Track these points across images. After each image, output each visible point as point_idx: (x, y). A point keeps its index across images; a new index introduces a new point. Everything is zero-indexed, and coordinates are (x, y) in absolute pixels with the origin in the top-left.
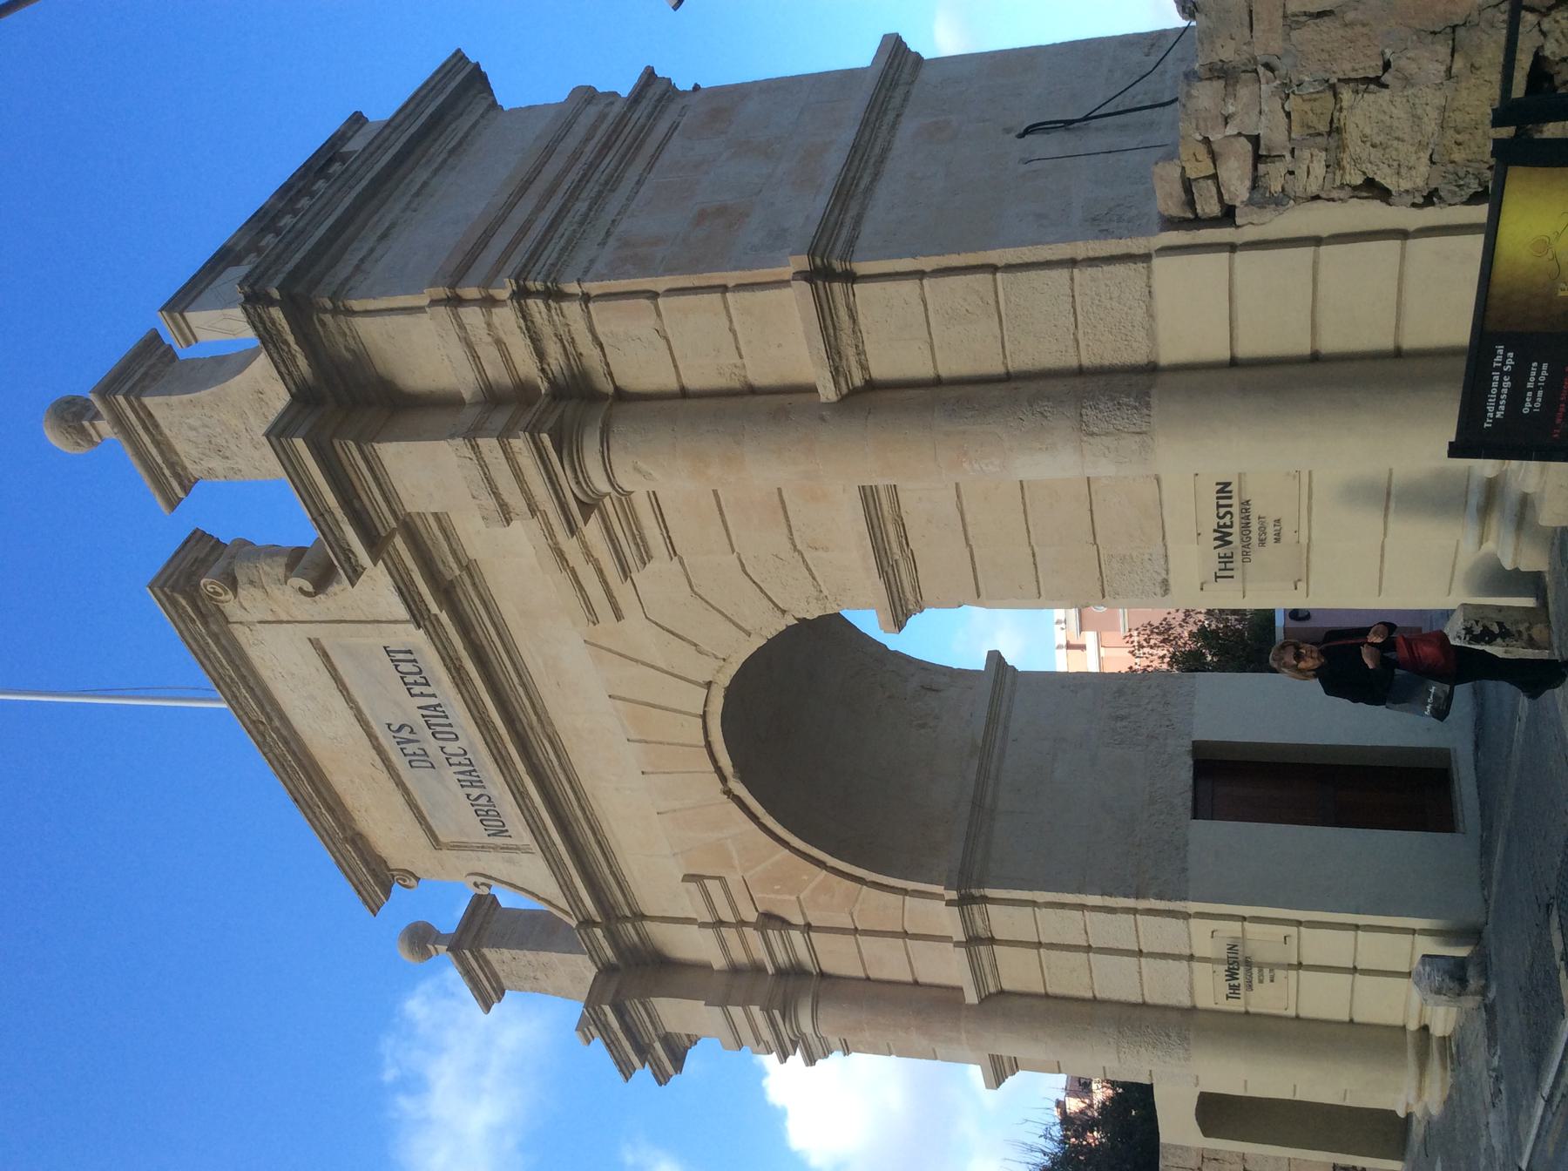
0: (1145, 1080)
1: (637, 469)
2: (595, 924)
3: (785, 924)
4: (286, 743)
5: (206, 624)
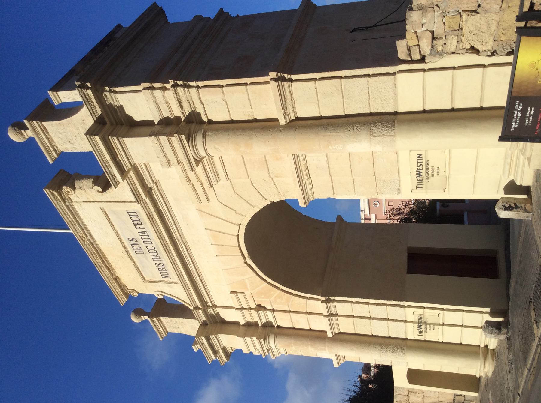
2: (199, 308)
4: (92, 244)
5: (65, 202)
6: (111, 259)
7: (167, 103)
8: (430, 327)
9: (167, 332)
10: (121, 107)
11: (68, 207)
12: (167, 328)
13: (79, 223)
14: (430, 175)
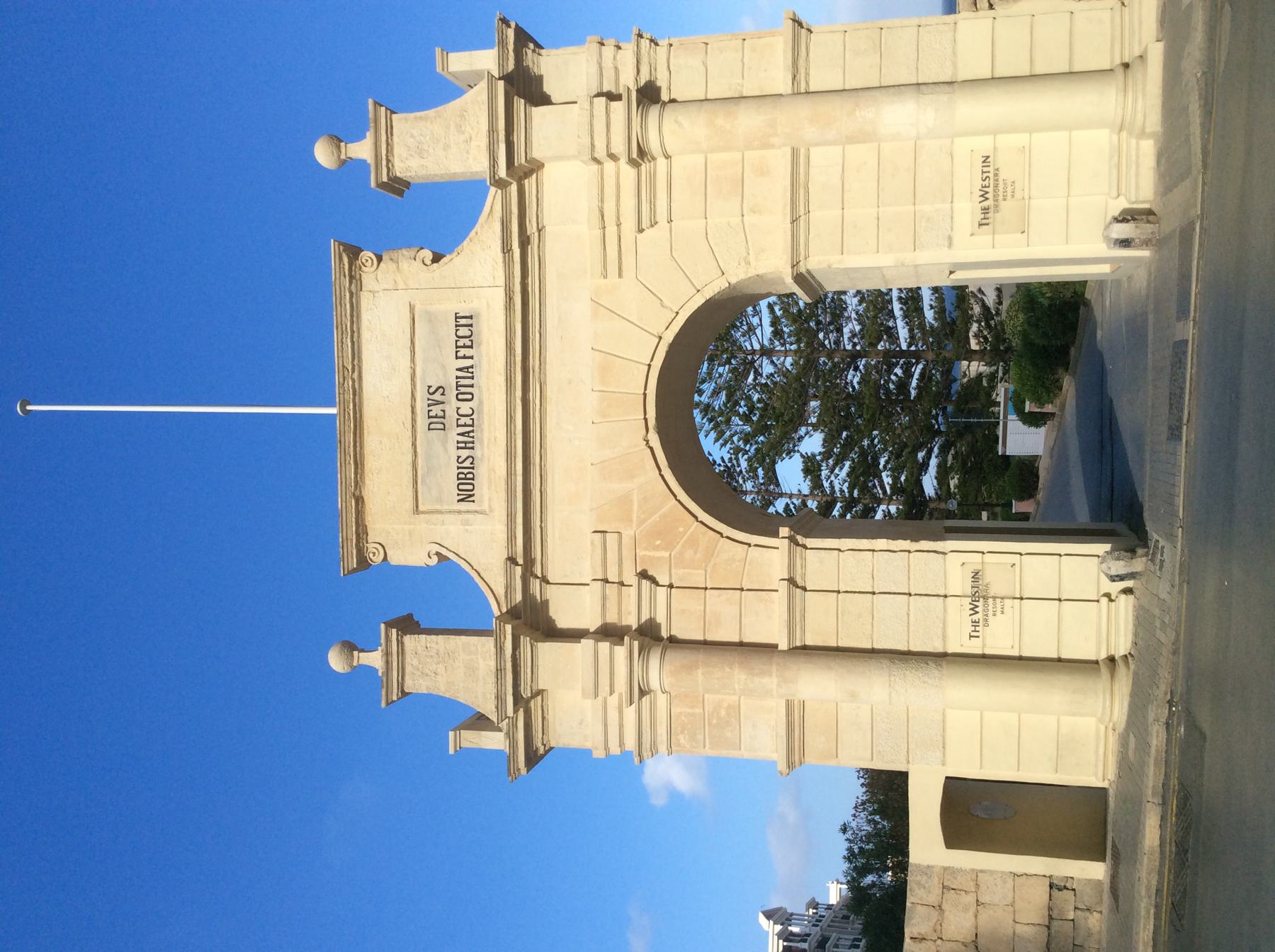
0: (904, 770)
2: (517, 564)
3: (654, 581)
4: (354, 395)
5: (351, 283)
6: (372, 442)
7: (616, 68)
8: (995, 604)
9: (403, 691)
10: (541, 77)
11: (351, 294)
12: (407, 678)
14: (1001, 198)
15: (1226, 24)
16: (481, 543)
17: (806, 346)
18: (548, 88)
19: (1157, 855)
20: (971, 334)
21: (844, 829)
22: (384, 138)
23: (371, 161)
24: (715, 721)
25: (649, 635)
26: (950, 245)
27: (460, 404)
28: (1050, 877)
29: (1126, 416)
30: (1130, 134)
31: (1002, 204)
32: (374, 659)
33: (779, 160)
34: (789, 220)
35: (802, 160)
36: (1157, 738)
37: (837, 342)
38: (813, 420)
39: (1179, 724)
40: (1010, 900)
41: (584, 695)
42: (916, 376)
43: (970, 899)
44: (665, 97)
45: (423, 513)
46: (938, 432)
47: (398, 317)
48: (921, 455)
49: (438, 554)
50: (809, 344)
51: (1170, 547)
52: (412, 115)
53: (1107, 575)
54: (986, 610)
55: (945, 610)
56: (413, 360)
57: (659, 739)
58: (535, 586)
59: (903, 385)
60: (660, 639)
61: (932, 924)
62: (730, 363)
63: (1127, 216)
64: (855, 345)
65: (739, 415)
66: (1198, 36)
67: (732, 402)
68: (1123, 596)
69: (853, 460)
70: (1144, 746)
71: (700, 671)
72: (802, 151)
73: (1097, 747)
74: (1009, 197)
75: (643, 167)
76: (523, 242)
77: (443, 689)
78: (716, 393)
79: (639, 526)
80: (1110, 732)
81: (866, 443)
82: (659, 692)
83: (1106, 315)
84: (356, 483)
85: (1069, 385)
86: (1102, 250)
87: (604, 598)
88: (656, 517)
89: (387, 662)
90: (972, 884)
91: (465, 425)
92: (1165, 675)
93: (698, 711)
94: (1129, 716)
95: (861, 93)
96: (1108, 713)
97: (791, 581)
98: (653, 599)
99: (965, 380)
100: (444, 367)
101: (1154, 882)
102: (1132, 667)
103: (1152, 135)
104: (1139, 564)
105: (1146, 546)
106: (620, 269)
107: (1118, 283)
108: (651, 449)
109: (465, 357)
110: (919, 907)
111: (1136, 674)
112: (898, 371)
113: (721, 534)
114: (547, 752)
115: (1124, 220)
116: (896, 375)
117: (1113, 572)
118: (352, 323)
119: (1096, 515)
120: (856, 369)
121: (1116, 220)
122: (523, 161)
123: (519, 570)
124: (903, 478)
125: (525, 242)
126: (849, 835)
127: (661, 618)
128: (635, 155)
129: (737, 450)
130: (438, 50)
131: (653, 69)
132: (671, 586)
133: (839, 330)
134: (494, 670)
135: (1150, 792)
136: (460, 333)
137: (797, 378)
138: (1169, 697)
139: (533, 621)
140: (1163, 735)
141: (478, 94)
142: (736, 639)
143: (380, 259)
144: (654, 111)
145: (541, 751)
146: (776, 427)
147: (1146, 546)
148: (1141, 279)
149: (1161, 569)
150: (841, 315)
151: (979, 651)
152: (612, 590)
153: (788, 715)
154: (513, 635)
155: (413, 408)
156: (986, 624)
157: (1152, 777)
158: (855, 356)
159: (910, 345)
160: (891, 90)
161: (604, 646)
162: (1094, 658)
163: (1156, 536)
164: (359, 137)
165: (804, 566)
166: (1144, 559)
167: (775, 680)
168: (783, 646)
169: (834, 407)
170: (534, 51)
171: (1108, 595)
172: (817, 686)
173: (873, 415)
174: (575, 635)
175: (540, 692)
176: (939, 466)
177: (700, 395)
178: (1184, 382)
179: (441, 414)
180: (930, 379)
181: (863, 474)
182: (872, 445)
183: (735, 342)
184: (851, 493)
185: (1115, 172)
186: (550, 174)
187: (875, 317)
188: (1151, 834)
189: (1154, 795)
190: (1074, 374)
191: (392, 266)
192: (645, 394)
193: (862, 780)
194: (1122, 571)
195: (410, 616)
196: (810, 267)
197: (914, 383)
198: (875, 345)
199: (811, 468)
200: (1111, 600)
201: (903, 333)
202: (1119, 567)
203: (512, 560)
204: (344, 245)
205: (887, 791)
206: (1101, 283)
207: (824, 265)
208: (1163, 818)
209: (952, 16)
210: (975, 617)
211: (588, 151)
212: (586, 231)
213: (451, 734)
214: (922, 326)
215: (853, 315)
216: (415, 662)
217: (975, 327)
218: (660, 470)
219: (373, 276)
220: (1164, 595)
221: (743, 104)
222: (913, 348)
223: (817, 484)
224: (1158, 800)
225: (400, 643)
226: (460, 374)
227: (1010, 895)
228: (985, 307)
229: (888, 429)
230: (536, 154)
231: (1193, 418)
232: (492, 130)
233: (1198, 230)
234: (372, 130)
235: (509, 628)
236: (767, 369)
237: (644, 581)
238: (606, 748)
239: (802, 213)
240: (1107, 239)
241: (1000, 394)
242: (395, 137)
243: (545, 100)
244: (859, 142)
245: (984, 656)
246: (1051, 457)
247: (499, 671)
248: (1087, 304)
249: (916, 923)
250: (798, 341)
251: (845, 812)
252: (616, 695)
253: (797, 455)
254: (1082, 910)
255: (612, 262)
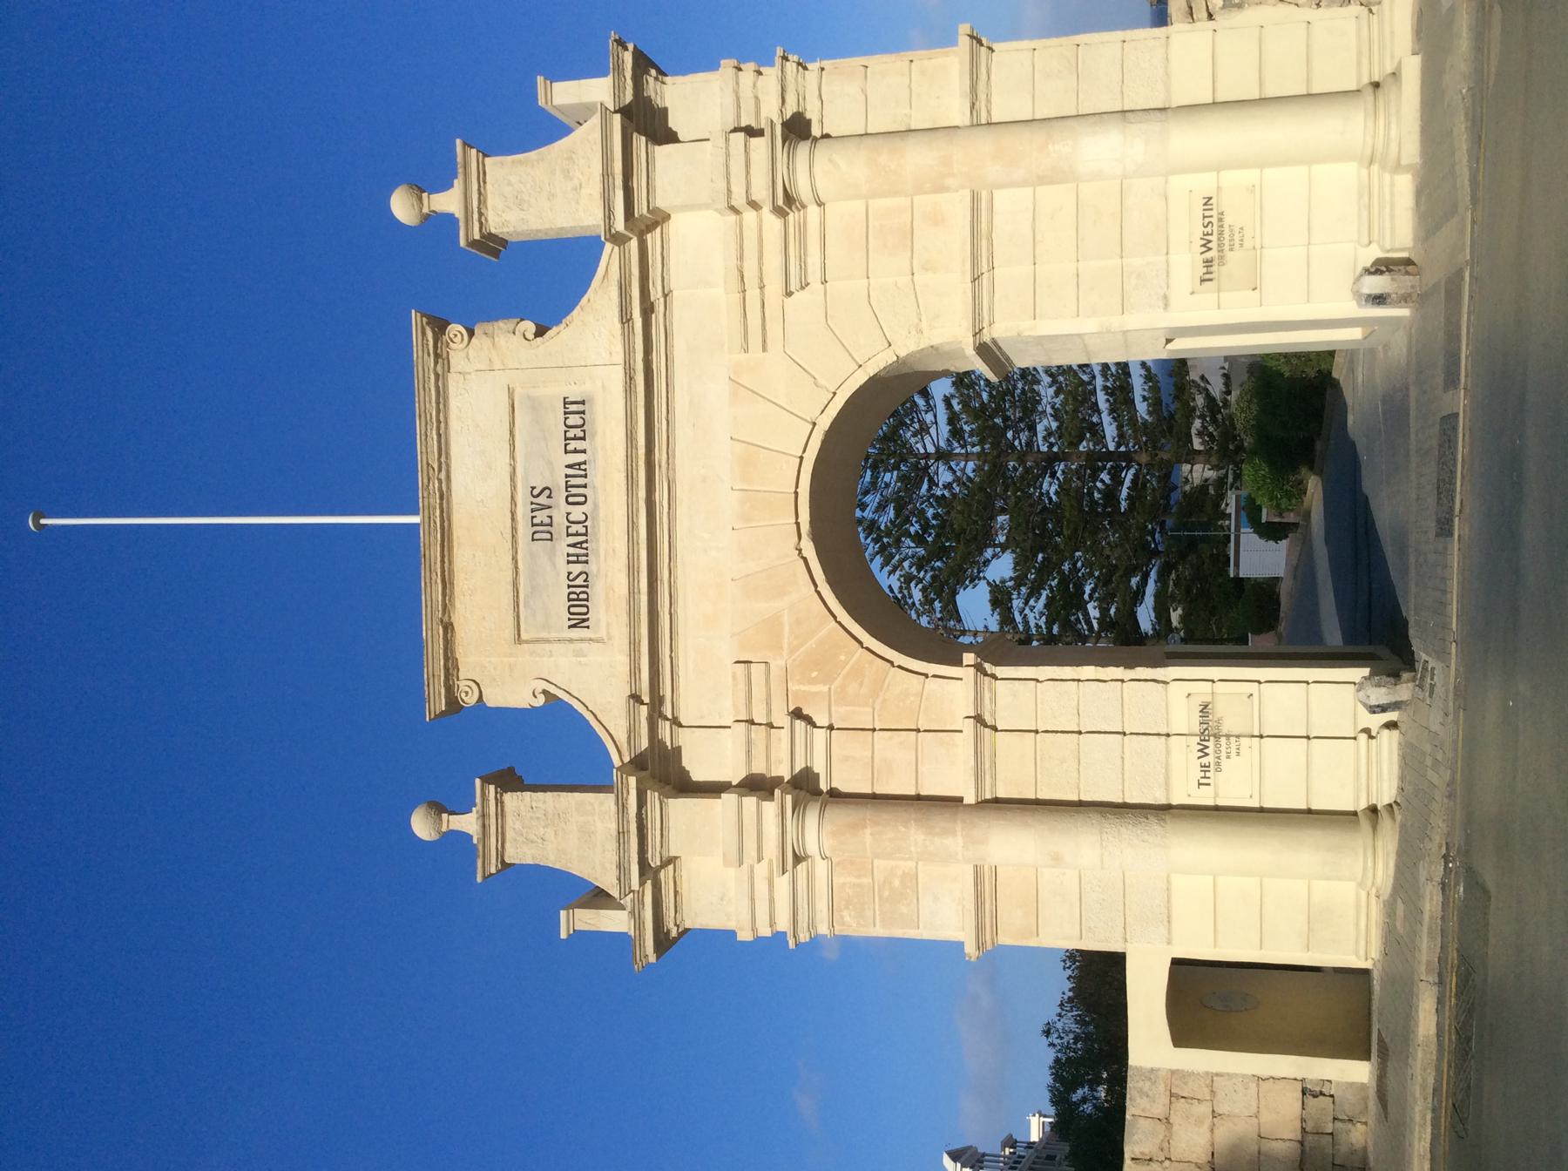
1: (830, 161)
3: (809, 720)
4: (441, 498)
5: (436, 363)
8: (1228, 744)
9: (503, 862)
10: (666, 109)
12: (508, 845)
13: (438, 428)
14: (1227, 247)
15: (1496, 31)
16: (597, 680)
17: (992, 448)
18: (673, 123)
19: (1434, 1047)
20: (1193, 432)
21: (1047, 1033)
22: (475, 187)
23: (459, 214)
24: (887, 893)
25: (805, 787)
26: (1166, 306)
27: (570, 508)
28: (1303, 1080)
29: (1385, 514)
30: (1383, 167)
31: (1229, 255)
32: (467, 823)
33: (956, 206)
34: (968, 278)
35: (984, 205)
36: (1431, 902)
37: (1030, 444)
38: (1002, 539)
39: (1457, 884)
40: (1254, 1109)
41: (726, 863)
42: (1127, 483)
43: (1205, 1109)
44: (816, 131)
45: (527, 642)
46: (1156, 553)
47: (490, 400)
48: (1134, 581)
49: (545, 692)
50: (995, 445)
51: (1442, 666)
52: (510, 158)
53: (1365, 705)
54: (1217, 751)
55: (1168, 752)
56: (512, 457)
57: (818, 916)
58: (665, 730)
59: (1111, 494)
60: (818, 793)
61: (1158, 1141)
62: (898, 468)
63: (1382, 267)
64: (1051, 445)
65: (908, 535)
66: (1463, 44)
67: (902, 518)
68: (1386, 732)
69: (1051, 588)
70: (1415, 913)
71: (868, 831)
72: (984, 195)
73: (1357, 942)
74: (1237, 246)
75: (791, 216)
76: (645, 309)
77: (552, 858)
78: (881, 507)
79: (792, 652)
80: (1373, 900)
81: (1066, 567)
82: (818, 858)
83: (1359, 393)
84: (445, 606)
85: (1314, 486)
86: (1352, 309)
87: (749, 743)
88: (811, 643)
89: (484, 826)
90: (1207, 1091)
91: (577, 534)
92: (1439, 825)
93: (867, 881)
94: (1396, 878)
95: (1054, 123)
96: (1370, 874)
97: (979, 719)
98: (809, 745)
99: (1187, 488)
100: (550, 463)
101: (1431, 1080)
102: (1398, 817)
103: (1409, 168)
104: (1404, 691)
105: (1412, 668)
106: (764, 341)
107: (1372, 352)
108: (805, 559)
109: (576, 451)
110: (1142, 1121)
111: (1403, 827)
112: (1105, 476)
113: (891, 663)
114: (681, 935)
115: (1378, 272)
116: (1102, 481)
117: (1373, 702)
118: (438, 411)
119: (1350, 636)
120: (1053, 475)
121: (1368, 272)
122: (645, 211)
123: (644, 710)
124: (1112, 611)
125: (648, 310)
126: (1054, 1038)
127: (819, 767)
128: (780, 202)
129: (908, 579)
130: (540, 79)
131: (801, 97)
132: (831, 728)
133: (1032, 428)
134: (615, 833)
135: (1423, 968)
136: (569, 422)
137: (982, 489)
138: (1444, 851)
139: (663, 772)
140: (1438, 898)
141: (592, 126)
142: (912, 792)
143: (471, 333)
144: (803, 148)
145: (674, 933)
146: (953, 560)
147: (1412, 668)
148: (1400, 345)
149: (1432, 693)
150: (1034, 410)
151: (1210, 803)
152: (758, 733)
153: (976, 885)
154: (638, 789)
155: (513, 514)
156: (1218, 769)
157: (1427, 951)
158: (1051, 459)
159: (1119, 445)
160: (1092, 119)
161: (750, 802)
162: (1351, 808)
163: (1424, 657)
164: (446, 185)
165: (994, 701)
166: (1411, 685)
167: (960, 840)
168: (970, 799)
169: (1028, 522)
170: (656, 79)
171: (1367, 731)
172: (1012, 846)
173: (1076, 530)
174: (714, 789)
175: (672, 860)
176: (1157, 596)
177: (863, 510)
178: (1455, 465)
179: (547, 521)
180: (1144, 485)
181: (1064, 608)
182: (1074, 569)
183: (905, 444)
184: (1050, 629)
185: (1365, 213)
186: (682, 228)
187: (1076, 411)
188: (1426, 1021)
189: (1428, 971)
190: (1320, 473)
191: (486, 341)
192: (796, 493)
193: (1069, 972)
194: (1384, 701)
195: (511, 770)
196: (995, 336)
197: (1124, 492)
198: (1076, 445)
199: (1000, 598)
200: (1371, 737)
201: (1110, 430)
202: (1379, 695)
203: (636, 698)
204: (428, 317)
205: (1098, 979)
206: (1352, 353)
207: (1014, 333)
208: (1440, 1001)
209: (1163, 29)
210: (1205, 761)
211: (723, 198)
212: (721, 294)
213: (563, 913)
214: (1133, 420)
215: (1049, 410)
216: (518, 825)
217: (1197, 424)
218: (816, 585)
219: (463, 354)
220: (1435, 727)
221: (912, 140)
222: (1123, 449)
223: (1007, 619)
224: (1434, 978)
225: (499, 802)
226: (570, 471)
227: (1254, 1104)
228: (1210, 399)
229: (1095, 549)
230: (661, 202)
231: (1467, 511)
232: (607, 174)
233: (1467, 278)
234: (461, 176)
235: (632, 781)
236: (945, 476)
237: (798, 722)
238: (754, 929)
239: (985, 268)
240: (1357, 295)
241: (1230, 504)
242: (489, 186)
243: (672, 138)
244: (1052, 182)
245: (1217, 808)
246: (1295, 578)
247: (621, 834)
248: (1335, 385)
249: (1134, 1145)
250: (982, 442)
251: (1049, 1010)
252: (764, 863)
253: (983, 583)
254: (1342, 1121)
255: (754, 332)
